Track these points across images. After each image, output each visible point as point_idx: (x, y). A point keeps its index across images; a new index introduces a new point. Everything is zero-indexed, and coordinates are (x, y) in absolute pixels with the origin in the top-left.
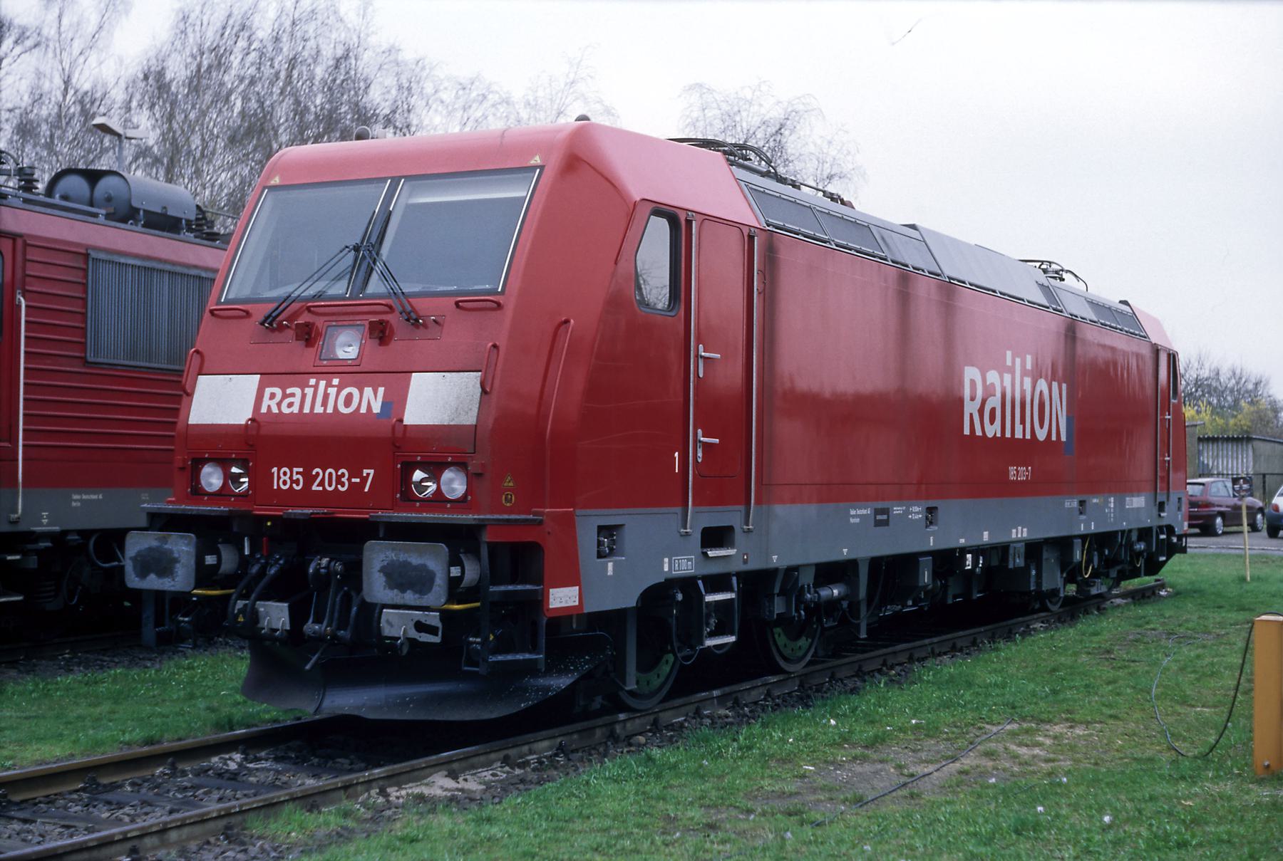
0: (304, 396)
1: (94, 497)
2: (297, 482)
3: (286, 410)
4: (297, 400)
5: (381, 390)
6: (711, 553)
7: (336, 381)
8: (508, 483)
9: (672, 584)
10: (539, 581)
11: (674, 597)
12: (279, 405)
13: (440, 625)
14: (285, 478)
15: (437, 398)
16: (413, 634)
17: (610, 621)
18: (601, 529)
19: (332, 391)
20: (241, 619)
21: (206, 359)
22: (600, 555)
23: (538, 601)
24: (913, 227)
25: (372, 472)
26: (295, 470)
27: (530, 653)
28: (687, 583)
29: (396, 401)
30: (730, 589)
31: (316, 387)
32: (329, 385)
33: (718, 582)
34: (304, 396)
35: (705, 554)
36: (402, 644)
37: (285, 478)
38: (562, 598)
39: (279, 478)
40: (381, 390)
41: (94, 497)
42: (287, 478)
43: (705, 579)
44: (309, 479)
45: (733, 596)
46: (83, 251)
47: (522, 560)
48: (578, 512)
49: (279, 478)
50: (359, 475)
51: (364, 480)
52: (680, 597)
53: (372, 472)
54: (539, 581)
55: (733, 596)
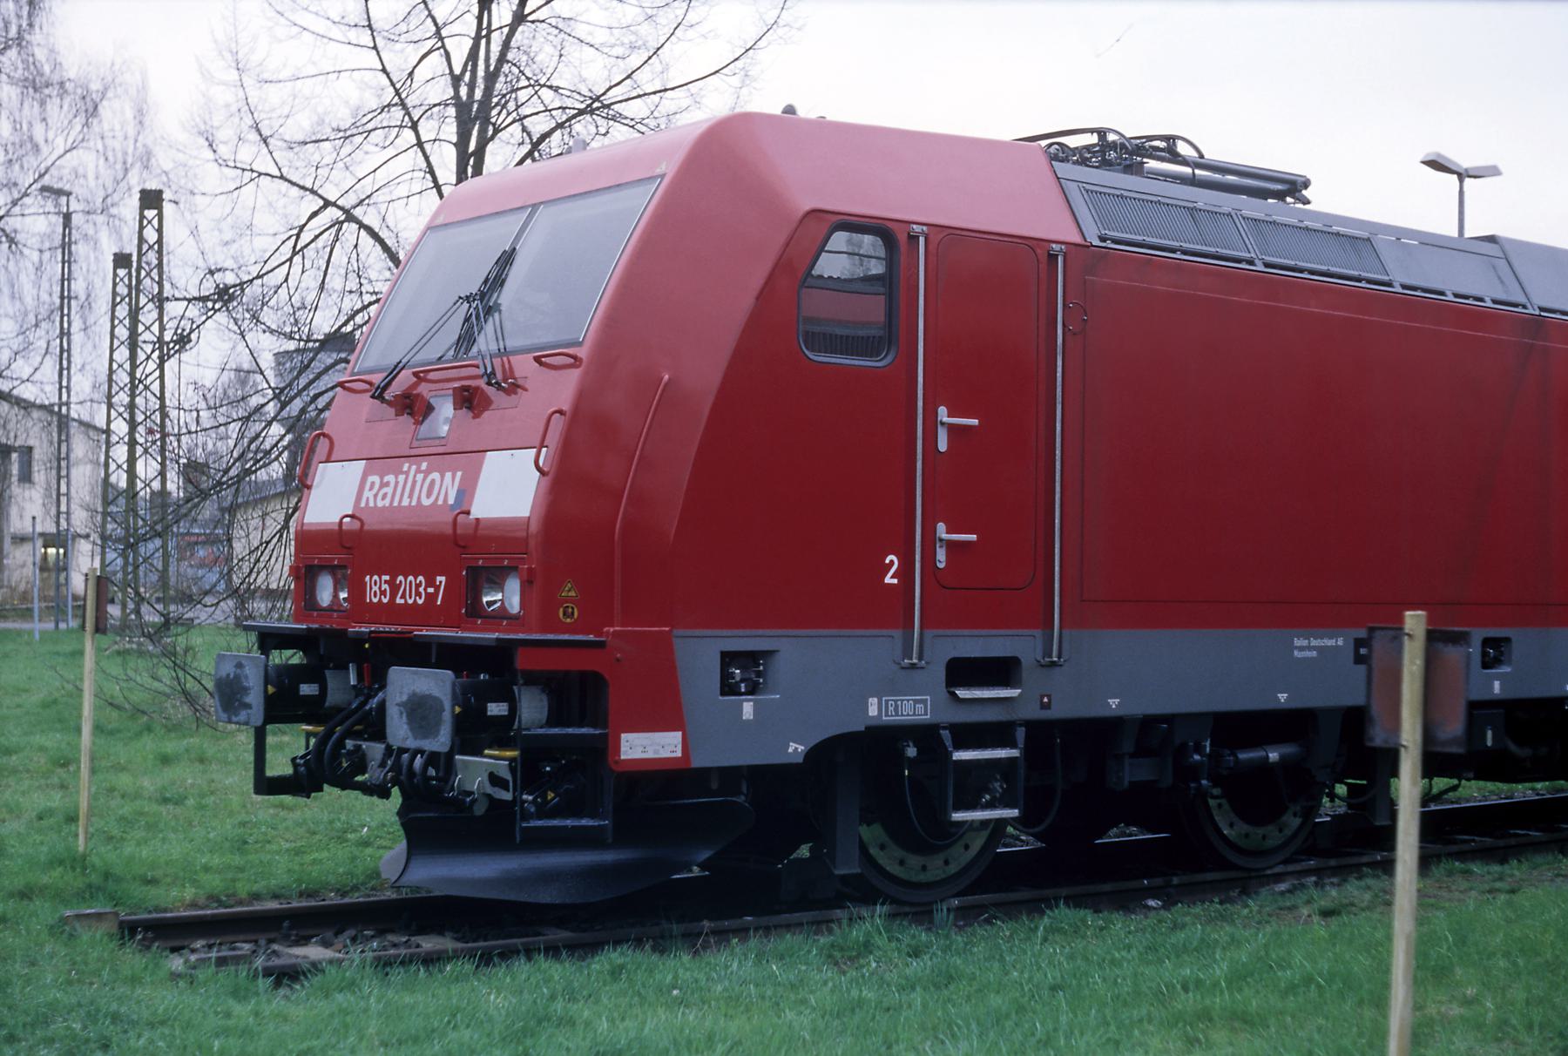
0: (397, 483)
1: (1330, 643)
3: (380, 504)
4: (389, 490)
5: (459, 474)
6: (962, 693)
7: (424, 466)
8: (569, 591)
9: (885, 738)
10: (599, 720)
11: (902, 753)
12: (376, 496)
13: (509, 777)
14: (376, 588)
15: (509, 488)
16: (489, 790)
17: (766, 780)
18: (728, 658)
19: (420, 477)
20: (432, 772)
21: (335, 438)
22: (728, 688)
23: (603, 748)
24: (1491, 239)
25: (443, 579)
27: (592, 817)
28: (924, 734)
29: (467, 491)
30: (1012, 744)
31: (407, 473)
32: (418, 471)
34: (397, 483)
35: (954, 694)
36: (474, 801)
37: (376, 588)
38: (643, 746)
40: (459, 474)
41: (1330, 643)
42: (376, 588)
43: (953, 728)
44: (395, 588)
45: (1014, 753)
46: (1365, 235)
47: (581, 695)
48: (676, 632)
51: (437, 588)
52: (911, 752)
53: (443, 579)
54: (599, 720)
55: (1014, 753)
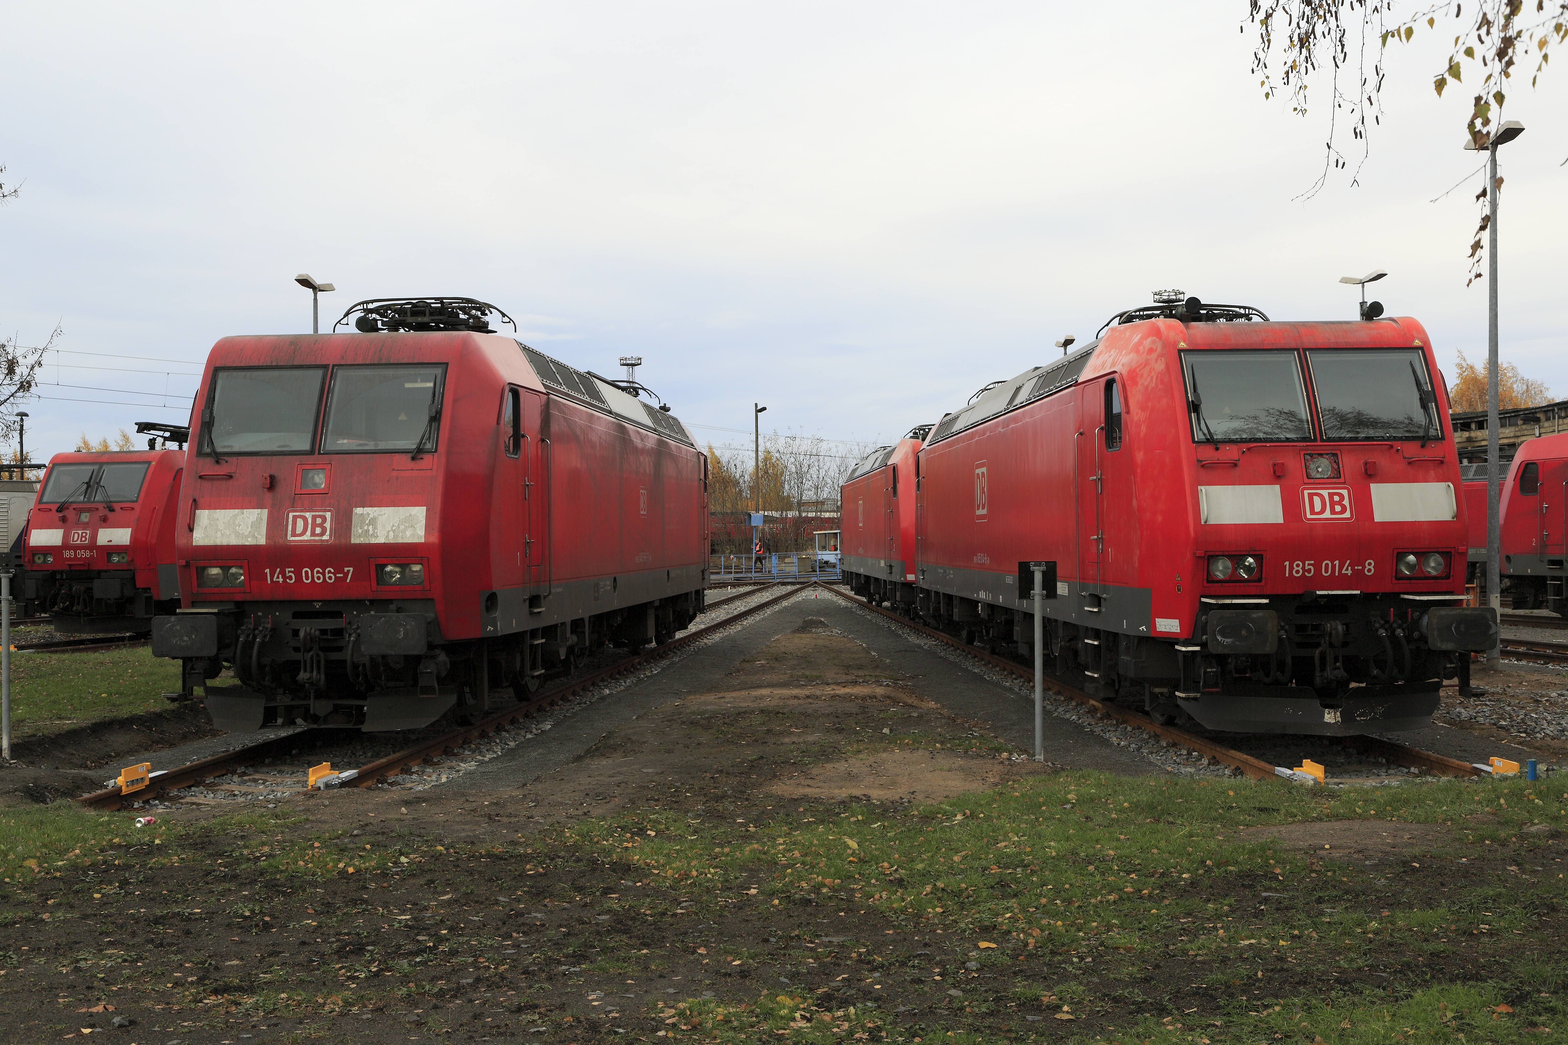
2: (1309, 571)
26: (1307, 562)
33: (534, 634)
39: (1291, 568)
42: (1300, 569)
49: (1291, 568)
50: (342, 572)
